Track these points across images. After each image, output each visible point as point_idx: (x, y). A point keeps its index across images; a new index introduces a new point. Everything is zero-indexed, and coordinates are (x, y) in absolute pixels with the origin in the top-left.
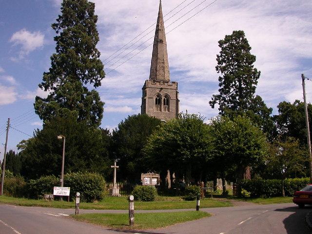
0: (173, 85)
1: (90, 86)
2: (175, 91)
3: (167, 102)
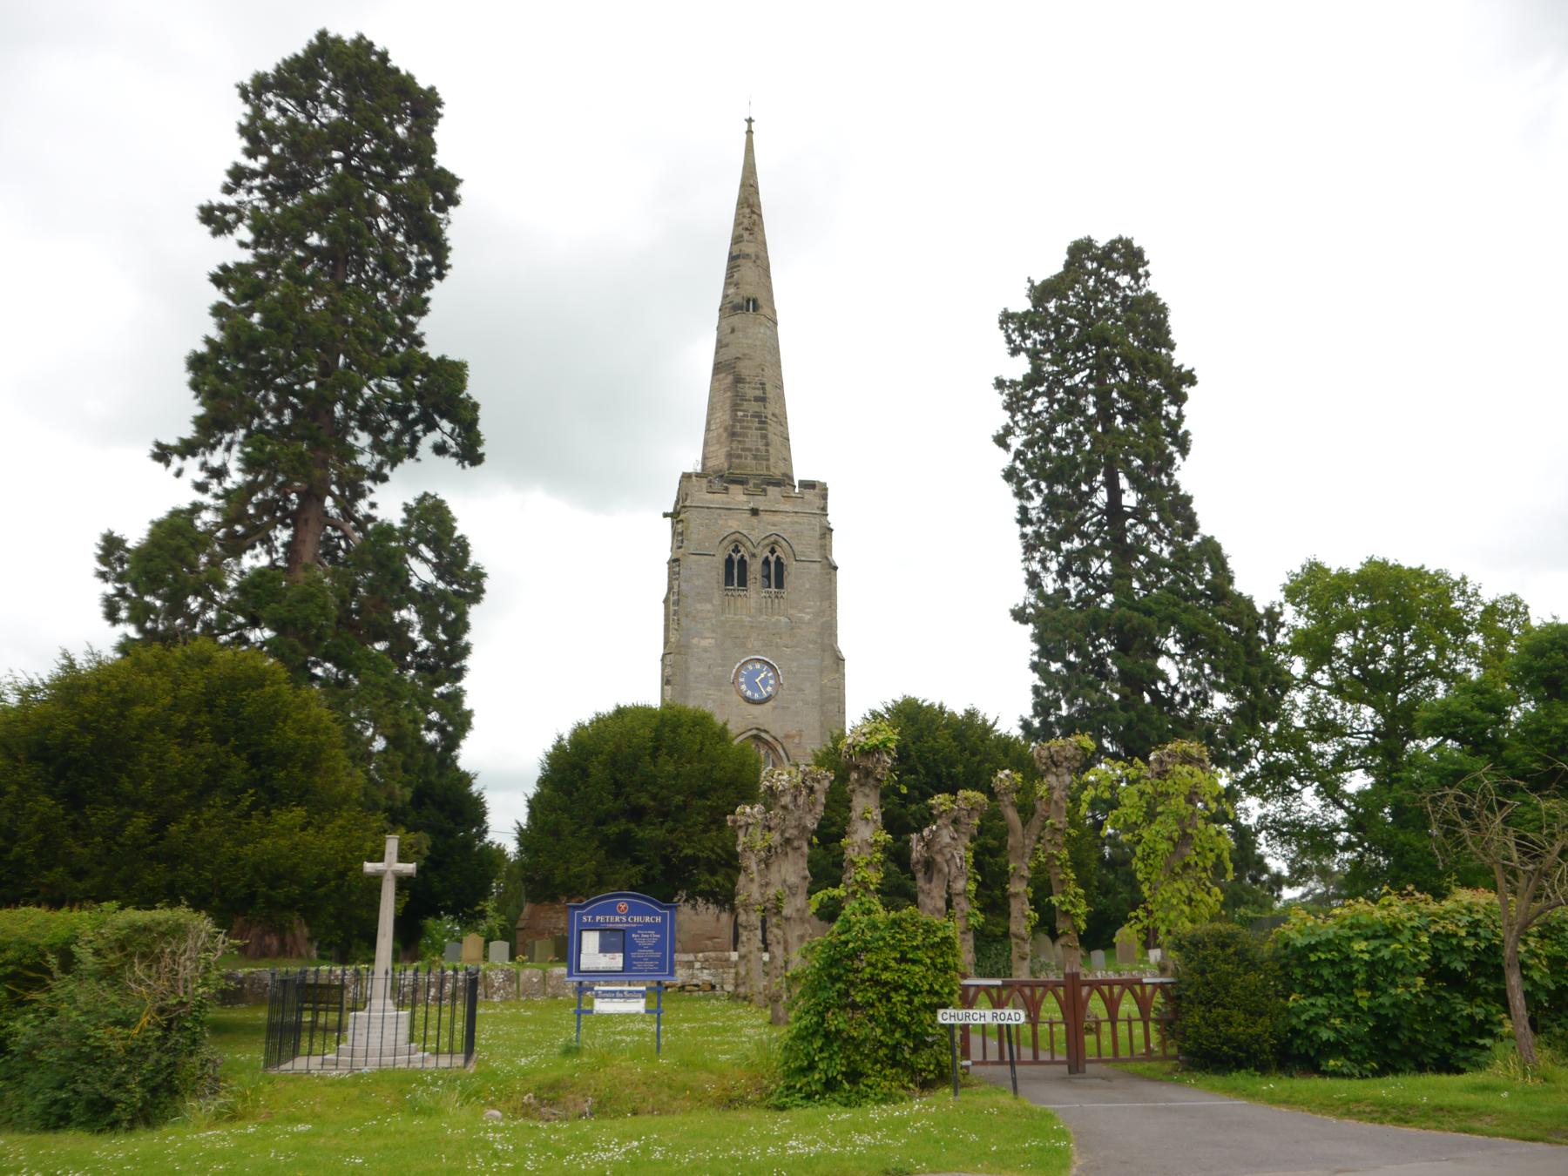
2: (815, 521)
3: (776, 574)
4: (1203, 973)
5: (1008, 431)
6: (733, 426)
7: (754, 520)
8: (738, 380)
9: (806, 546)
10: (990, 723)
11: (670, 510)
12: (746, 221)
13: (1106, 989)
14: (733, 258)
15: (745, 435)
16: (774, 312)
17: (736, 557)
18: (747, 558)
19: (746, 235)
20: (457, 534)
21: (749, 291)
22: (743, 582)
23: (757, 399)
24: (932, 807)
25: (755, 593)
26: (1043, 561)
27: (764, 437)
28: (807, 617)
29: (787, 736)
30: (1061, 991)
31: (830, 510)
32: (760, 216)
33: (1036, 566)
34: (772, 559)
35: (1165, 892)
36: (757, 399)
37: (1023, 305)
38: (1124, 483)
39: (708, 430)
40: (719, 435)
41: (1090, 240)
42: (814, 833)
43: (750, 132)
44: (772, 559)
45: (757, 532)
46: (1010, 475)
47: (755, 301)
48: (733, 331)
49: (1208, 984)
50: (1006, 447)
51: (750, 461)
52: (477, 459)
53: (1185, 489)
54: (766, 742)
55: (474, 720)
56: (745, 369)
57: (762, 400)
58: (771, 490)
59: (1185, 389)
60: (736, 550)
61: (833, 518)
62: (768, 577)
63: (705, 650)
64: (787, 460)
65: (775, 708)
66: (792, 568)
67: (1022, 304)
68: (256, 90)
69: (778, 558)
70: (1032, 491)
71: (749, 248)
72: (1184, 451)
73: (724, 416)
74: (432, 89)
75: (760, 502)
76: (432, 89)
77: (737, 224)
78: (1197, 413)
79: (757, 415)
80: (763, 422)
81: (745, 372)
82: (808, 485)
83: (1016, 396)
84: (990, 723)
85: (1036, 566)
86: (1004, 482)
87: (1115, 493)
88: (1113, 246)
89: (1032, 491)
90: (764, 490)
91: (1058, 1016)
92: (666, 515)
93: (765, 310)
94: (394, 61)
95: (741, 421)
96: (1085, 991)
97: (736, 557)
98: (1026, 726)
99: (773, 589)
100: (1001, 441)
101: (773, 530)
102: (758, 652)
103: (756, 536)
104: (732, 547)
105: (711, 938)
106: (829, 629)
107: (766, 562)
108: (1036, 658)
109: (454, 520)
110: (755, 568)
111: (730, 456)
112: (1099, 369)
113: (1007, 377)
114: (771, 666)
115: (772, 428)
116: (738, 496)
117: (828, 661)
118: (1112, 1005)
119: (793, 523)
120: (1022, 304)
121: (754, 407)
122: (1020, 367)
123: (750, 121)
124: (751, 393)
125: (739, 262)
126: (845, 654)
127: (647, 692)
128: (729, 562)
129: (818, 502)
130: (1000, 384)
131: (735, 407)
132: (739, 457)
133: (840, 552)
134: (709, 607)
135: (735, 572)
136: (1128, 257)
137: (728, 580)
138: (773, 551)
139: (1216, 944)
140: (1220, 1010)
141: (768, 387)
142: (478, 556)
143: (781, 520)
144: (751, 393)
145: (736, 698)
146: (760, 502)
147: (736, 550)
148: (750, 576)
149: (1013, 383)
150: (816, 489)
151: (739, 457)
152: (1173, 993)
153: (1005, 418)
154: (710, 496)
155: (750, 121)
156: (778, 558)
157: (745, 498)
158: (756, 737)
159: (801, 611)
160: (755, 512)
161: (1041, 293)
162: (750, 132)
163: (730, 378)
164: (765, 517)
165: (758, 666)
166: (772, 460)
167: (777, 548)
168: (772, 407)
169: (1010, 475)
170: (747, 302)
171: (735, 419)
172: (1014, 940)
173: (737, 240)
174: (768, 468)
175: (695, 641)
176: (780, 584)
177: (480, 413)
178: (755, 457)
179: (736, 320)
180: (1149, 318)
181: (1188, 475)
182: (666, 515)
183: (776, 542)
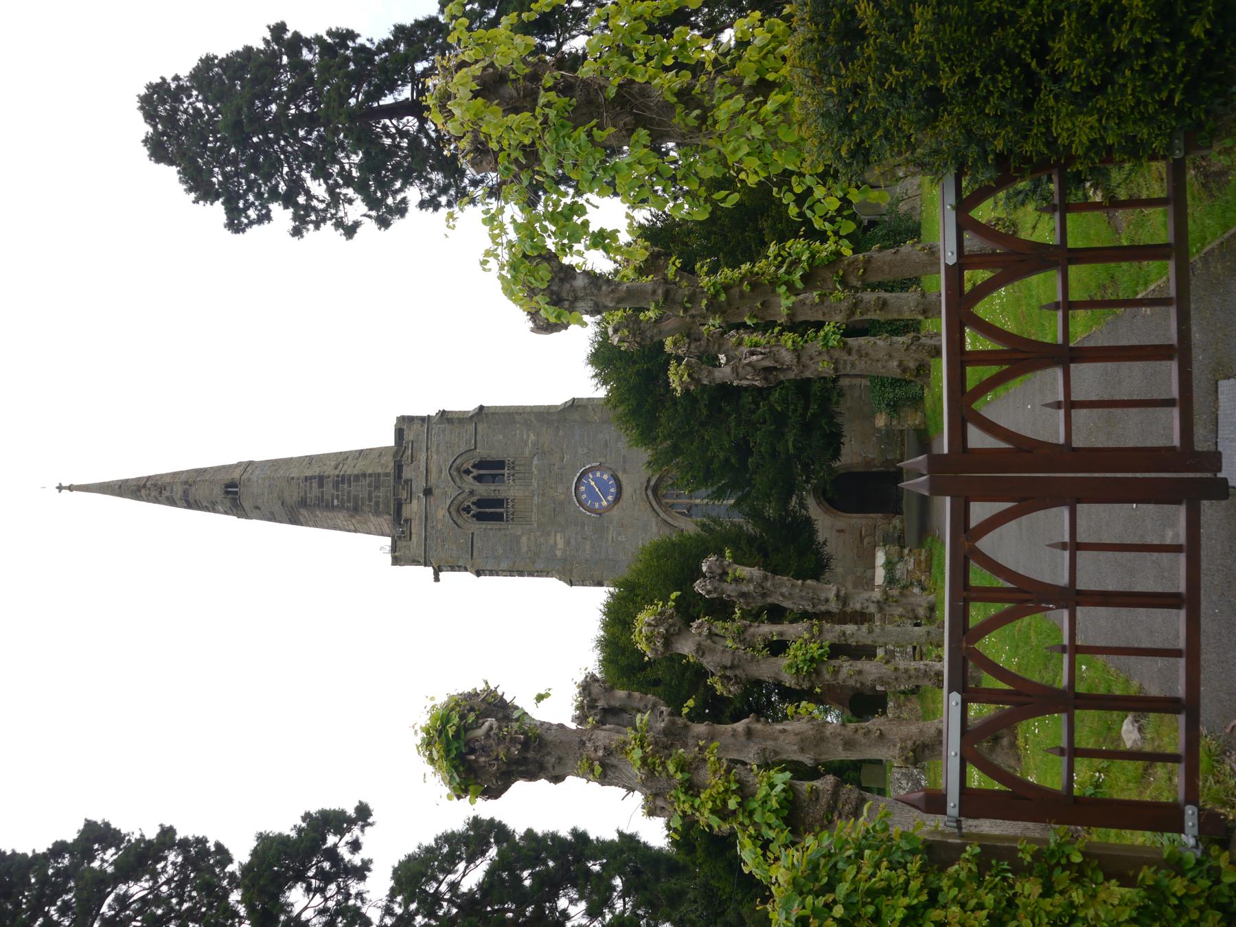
0: (409, 436)
2: (435, 429)
3: (490, 469)
4: (935, 98)
5: (339, 224)
6: (348, 509)
7: (436, 492)
8: (303, 503)
11: (430, 570)
12: (153, 494)
13: (975, 375)
14: (189, 505)
15: (356, 498)
16: (240, 464)
17: (475, 510)
18: (475, 499)
19: (166, 494)
20: (433, 844)
21: (218, 491)
22: (499, 503)
23: (321, 485)
24: (686, 392)
25: (510, 490)
27: (357, 478)
28: (532, 437)
30: (980, 511)
32: (149, 478)
34: (475, 472)
35: (737, 150)
36: (321, 485)
37: (217, 211)
38: (388, 100)
39: (356, 531)
40: (359, 522)
41: (145, 141)
42: (676, 705)
43: (71, 488)
44: (475, 472)
45: (447, 490)
46: (384, 223)
47: (227, 486)
48: (257, 508)
49: (970, 82)
50: (357, 225)
51: (381, 493)
52: (363, 813)
53: (385, 33)
56: (293, 495)
57: (321, 479)
58: (407, 473)
59: (288, 35)
60: (467, 510)
62: (494, 476)
63: (568, 543)
64: (381, 452)
65: (625, 471)
66: (482, 452)
69: (474, 466)
70: (399, 197)
71: (178, 491)
72: (352, 35)
73: (341, 517)
75: (419, 485)
77: (156, 500)
78: (311, 23)
79: (336, 485)
80: (342, 480)
81: (296, 497)
82: (399, 433)
83: (303, 220)
86: (391, 228)
87: (398, 110)
88: (150, 116)
89: (399, 197)
91: (1054, 521)
92: (437, 579)
93: (236, 475)
95: (343, 503)
96: (977, 439)
97: (475, 510)
99: (506, 471)
100: (350, 231)
101: (445, 473)
102: (569, 488)
103: (453, 492)
104: (465, 515)
105: (862, 539)
106: (542, 416)
107: (479, 479)
110: (483, 490)
111: (377, 513)
112: (254, 131)
113: (291, 224)
114: (583, 474)
115: (349, 470)
116: (414, 509)
117: (576, 416)
118: (1022, 356)
119: (438, 452)
121: (328, 489)
122: (282, 216)
123: (60, 488)
124: (315, 491)
125: (191, 498)
126: (568, 398)
128: (480, 517)
129: (416, 426)
130: (297, 232)
131: (329, 507)
132: (377, 504)
133: (466, 404)
134: (524, 539)
135: (489, 511)
136: (158, 101)
137: (498, 517)
138: (468, 472)
139: (847, 56)
140: (1059, 46)
141: (309, 473)
143: (434, 464)
144: (315, 491)
145: (615, 511)
146: (419, 485)
147: (467, 510)
148: (493, 495)
149: (296, 217)
151: (377, 504)
152: (986, 176)
153: (328, 227)
154: (414, 536)
155: (60, 488)
156: (474, 466)
157: (415, 502)
158: (655, 490)
159: (526, 444)
160: (428, 492)
162: (71, 488)
163: (303, 511)
165: (583, 488)
166: (380, 470)
167: (465, 467)
168: (329, 471)
169: (384, 223)
170: (228, 491)
171: (341, 507)
172: (857, 317)
173: (171, 502)
174: (387, 475)
175: (559, 553)
176: (500, 464)
178: (377, 488)
179: (246, 505)
180: (210, 75)
181: (373, 29)
182: (437, 579)
183: (458, 470)
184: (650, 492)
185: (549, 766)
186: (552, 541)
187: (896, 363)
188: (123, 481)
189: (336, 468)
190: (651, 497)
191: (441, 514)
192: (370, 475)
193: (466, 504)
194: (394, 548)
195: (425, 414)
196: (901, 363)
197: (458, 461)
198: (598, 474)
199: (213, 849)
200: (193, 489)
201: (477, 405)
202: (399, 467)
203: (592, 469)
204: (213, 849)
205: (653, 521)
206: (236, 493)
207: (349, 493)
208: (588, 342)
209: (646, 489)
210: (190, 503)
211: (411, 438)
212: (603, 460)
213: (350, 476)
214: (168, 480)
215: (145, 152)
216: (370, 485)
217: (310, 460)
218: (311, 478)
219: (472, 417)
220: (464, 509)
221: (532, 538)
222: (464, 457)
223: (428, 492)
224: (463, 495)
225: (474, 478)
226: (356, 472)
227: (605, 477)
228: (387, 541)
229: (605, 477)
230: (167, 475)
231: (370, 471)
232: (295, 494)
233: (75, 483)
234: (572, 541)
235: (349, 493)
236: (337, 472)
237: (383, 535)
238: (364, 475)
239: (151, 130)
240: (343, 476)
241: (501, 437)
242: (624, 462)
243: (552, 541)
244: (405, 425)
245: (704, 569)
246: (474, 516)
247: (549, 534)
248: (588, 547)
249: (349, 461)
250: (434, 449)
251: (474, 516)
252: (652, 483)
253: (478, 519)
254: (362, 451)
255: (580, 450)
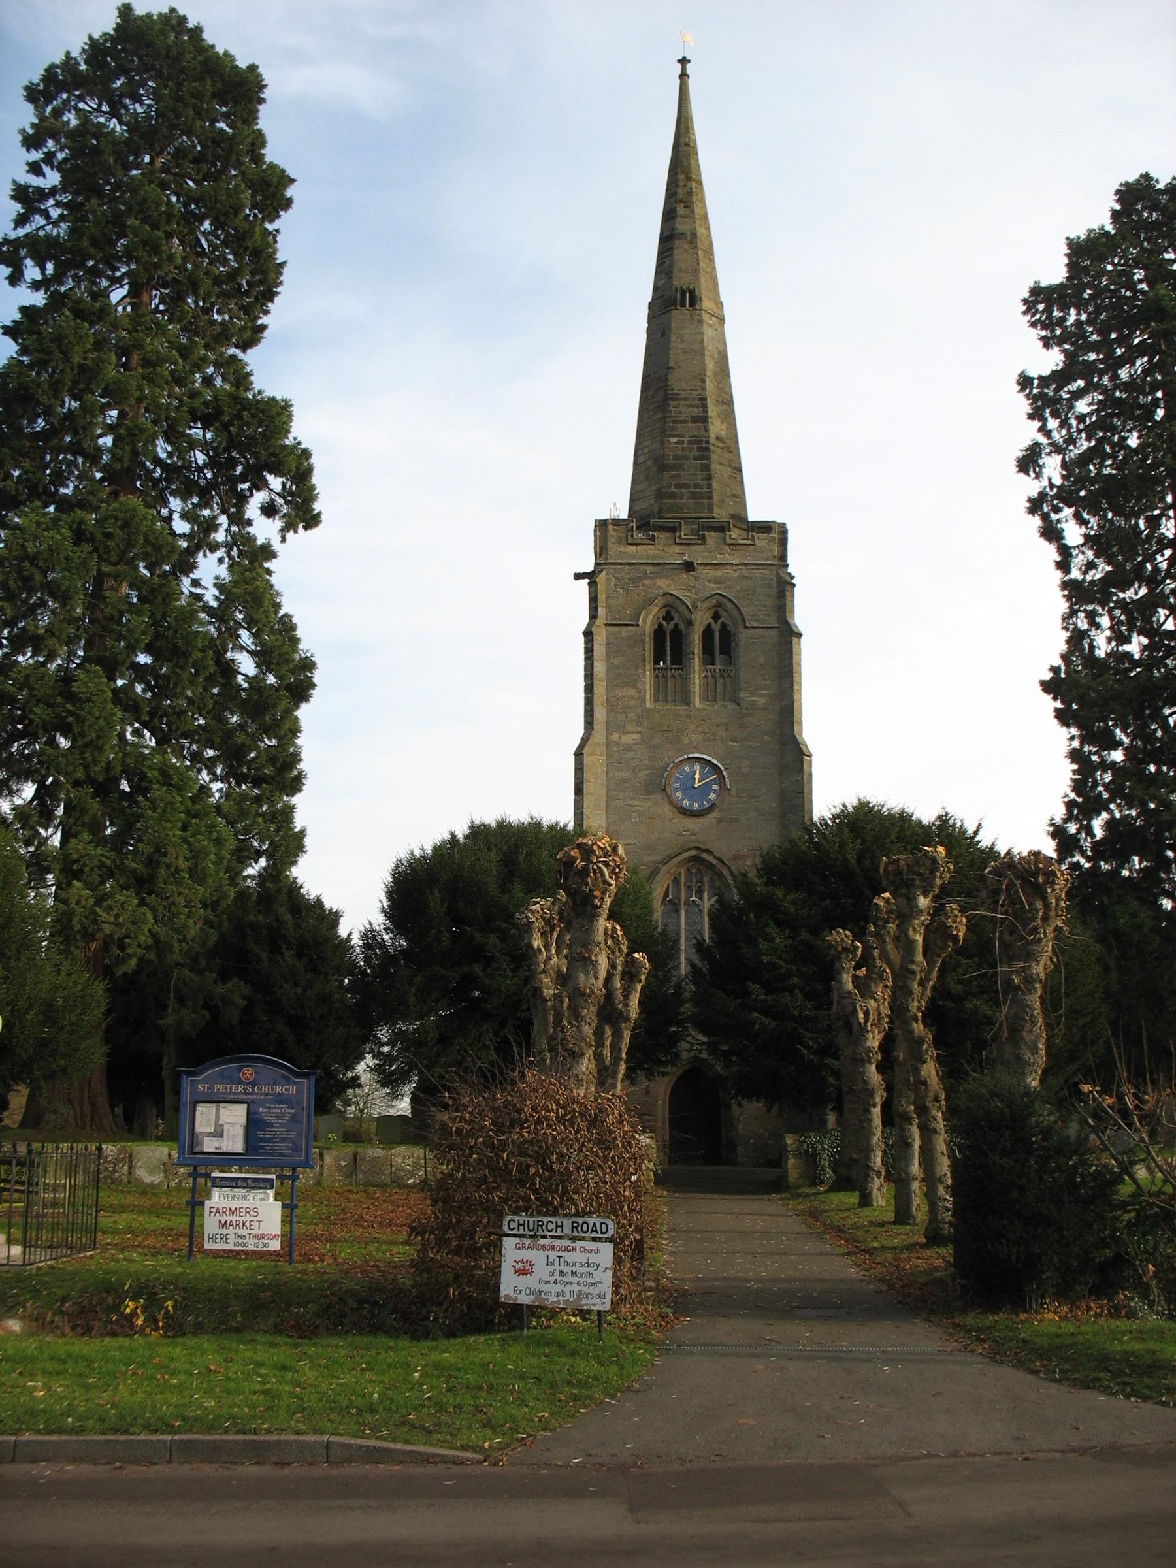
0: (761, 540)
1: (1067, 346)
9: (755, 610)
10: (970, 831)
11: (589, 568)
15: (679, 467)
16: (720, 305)
17: (669, 627)
18: (682, 626)
22: (679, 657)
23: (695, 419)
26: (1091, 617)
27: (706, 468)
28: (762, 701)
29: (736, 858)
31: (790, 561)
32: (700, 183)
33: (1083, 624)
34: (716, 627)
36: (695, 419)
41: (1146, 177)
43: (683, 76)
44: (716, 627)
46: (1035, 506)
54: (710, 866)
55: (307, 841)
58: (711, 537)
61: (795, 566)
63: (629, 748)
64: (739, 498)
65: (719, 821)
67: (1055, 273)
68: (49, 88)
74: (253, 68)
75: (697, 555)
76: (253, 68)
82: (765, 527)
83: (1044, 397)
84: (970, 831)
85: (1083, 624)
90: (703, 538)
92: (578, 576)
93: (706, 304)
94: (209, 37)
98: (1057, 832)
101: (713, 588)
107: (708, 633)
108: (1076, 744)
109: (278, 594)
111: (660, 495)
113: (1033, 373)
115: (716, 456)
116: (666, 550)
120: (1055, 273)
121: (692, 429)
122: (1051, 360)
123: (684, 61)
124: (687, 412)
127: (557, 810)
128: (659, 633)
130: (1025, 382)
132: (673, 496)
133: (803, 614)
137: (658, 656)
138: (716, 617)
142: (309, 641)
145: (666, 809)
146: (697, 555)
147: (668, 617)
150: (775, 533)
151: (673, 496)
154: (632, 549)
155: (684, 61)
156: (723, 625)
159: (752, 694)
161: (1085, 253)
162: (683, 76)
164: (703, 572)
166: (716, 498)
167: (723, 613)
169: (1035, 506)
177: (314, 460)
178: (694, 496)
182: (578, 576)
183: (719, 605)
184: (693, 853)
185: (580, 920)
186: (629, 728)
187: (855, 1156)
188: (695, 147)
189: (718, 438)
190: (687, 854)
191: (664, 584)
192: (709, 486)
193: (676, 616)
194: (616, 522)
195: (789, 561)
196: (856, 1161)
197: (729, 605)
198: (716, 787)
199: (260, 322)
200: (686, 246)
201: (802, 629)
202: (722, 528)
203: (721, 780)
204: (260, 322)
205: (658, 858)
206: (683, 305)
207: (687, 458)
208: (881, 801)
209: (698, 848)
210: (669, 215)
211: (758, 543)
212: (733, 792)
213: (708, 458)
214: (697, 211)
215: (1132, 177)
216: (696, 486)
217: (727, 402)
218: (705, 406)
219: (787, 623)
220: (668, 613)
221: (633, 703)
222: (735, 612)
223: (689, 566)
224: (686, 612)
225: (709, 625)
226: (715, 467)
227: (712, 796)
228: (624, 515)
229: (712, 796)
230: (705, 207)
231: (715, 485)
232: (684, 385)
233: (692, 83)
234: (631, 755)
235: (687, 458)
236: (712, 440)
237: (633, 500)
238: (709, 478)
239: (1161, 186)
240: (708, 450)
241: (762, 660)
242: (731, 820)
243: (629, 728)
244: (775, 533)
245: (636, 955)
246: (660, 625)
247: (639, 724)
248: (623, 774)
249: (727, 455)
250: (745, 572)
251: (660, 625)
252: (705, 856)
253: (656, 632)
254: (740, 470)
255: (746, 762)
